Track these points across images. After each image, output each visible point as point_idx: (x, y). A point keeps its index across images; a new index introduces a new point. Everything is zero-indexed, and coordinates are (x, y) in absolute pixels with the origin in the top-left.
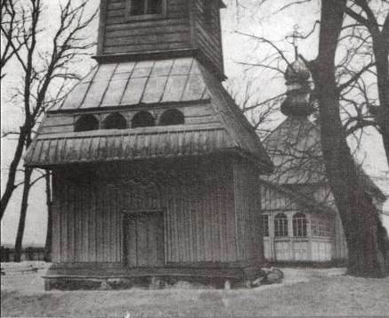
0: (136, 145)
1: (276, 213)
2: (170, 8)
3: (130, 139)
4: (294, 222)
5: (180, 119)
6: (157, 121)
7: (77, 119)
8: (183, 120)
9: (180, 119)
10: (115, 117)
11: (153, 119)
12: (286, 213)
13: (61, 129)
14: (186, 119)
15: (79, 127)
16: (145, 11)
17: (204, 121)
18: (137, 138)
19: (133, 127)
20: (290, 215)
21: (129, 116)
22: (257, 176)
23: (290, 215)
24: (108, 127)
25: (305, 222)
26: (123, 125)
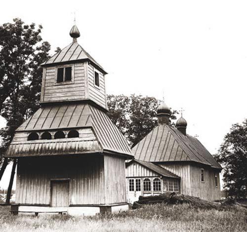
0: (55, 148)
1: (144, 179)
2: (76, 72)
3: (53, 144)
4: (154, 183)
5: (77, 135)
6: (66, 136)
7: (28, 134)
8: (17, 213)
9: (77, 135)
10: (46, 135)
11: (65, 135)
12: (150, 178)
13: (86, 135)
14: (19, 213)
15: (29, 138)
16: (64, 80)
17: (162, 142)
18: (56, 145)
19: (55, 138)
20: (152, 180)
21: (40, 135)
22: (25, 96)
23: (152, 180)
24: (42, 138)
25: (160, 183)
26: (50, 138)
